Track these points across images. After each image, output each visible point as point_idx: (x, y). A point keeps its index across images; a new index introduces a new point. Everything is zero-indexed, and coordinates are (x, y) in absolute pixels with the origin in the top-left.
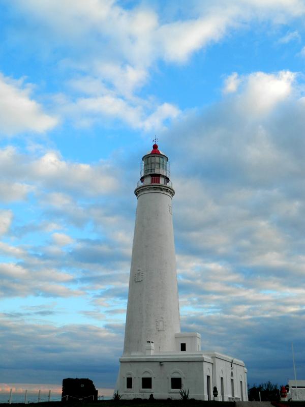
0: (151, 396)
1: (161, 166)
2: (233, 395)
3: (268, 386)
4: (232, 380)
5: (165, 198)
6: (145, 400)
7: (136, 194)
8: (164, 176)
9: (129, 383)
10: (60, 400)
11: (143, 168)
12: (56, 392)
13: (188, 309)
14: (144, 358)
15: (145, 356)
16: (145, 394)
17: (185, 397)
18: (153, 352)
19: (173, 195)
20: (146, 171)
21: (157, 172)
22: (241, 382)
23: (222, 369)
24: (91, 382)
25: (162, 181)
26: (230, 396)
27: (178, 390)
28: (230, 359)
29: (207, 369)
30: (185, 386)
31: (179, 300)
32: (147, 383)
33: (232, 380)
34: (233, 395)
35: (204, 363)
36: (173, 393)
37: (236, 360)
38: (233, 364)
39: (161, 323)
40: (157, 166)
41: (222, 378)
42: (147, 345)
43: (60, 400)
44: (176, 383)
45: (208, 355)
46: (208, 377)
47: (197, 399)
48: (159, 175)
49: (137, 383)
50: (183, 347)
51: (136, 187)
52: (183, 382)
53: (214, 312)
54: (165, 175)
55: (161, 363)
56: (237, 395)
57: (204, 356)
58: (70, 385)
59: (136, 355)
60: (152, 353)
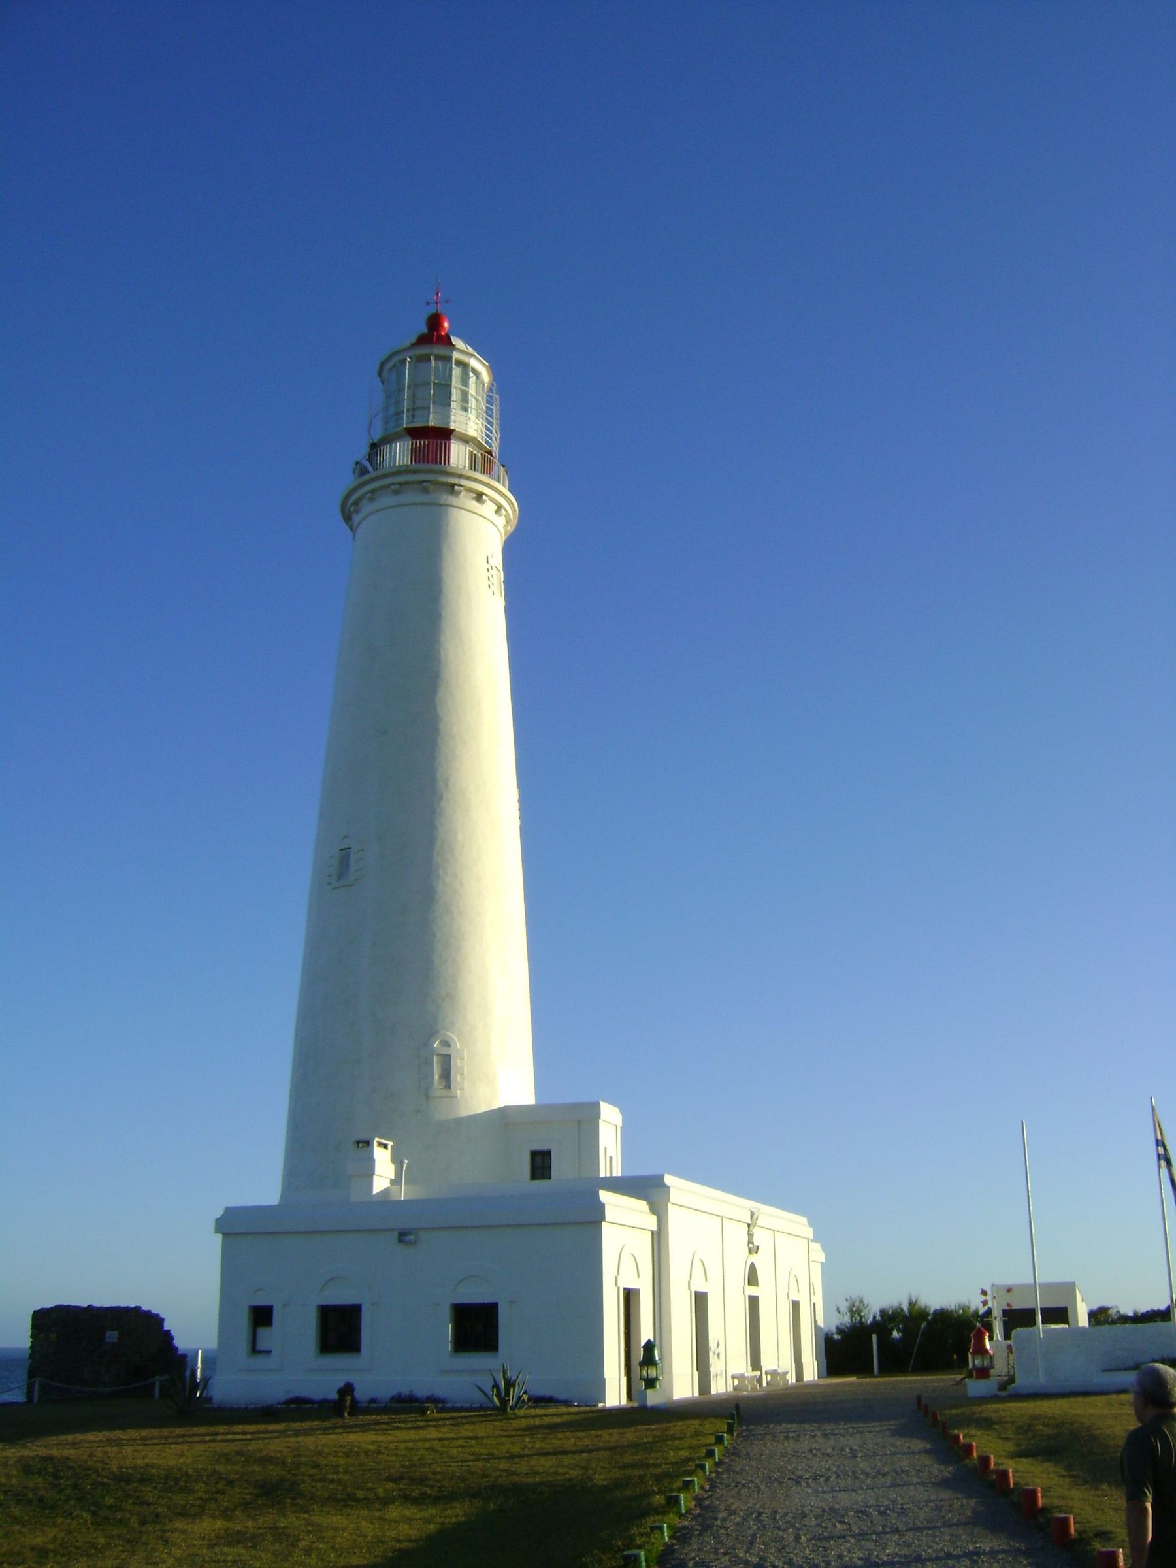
0: (347, 1389)
2: (756, 1362)
3: (851, 1311)
4: (753, 1302)
6: (323, 1402)
7: (347, 518)
16: (322, 1377)
22: (796, 1305)
33: (753, 1302)
34: (756, 1362)
36: (267, 1413)
38: (755, 1230)
44: (476, 1327)
46: (701, 1300)
49: (297, 1329)
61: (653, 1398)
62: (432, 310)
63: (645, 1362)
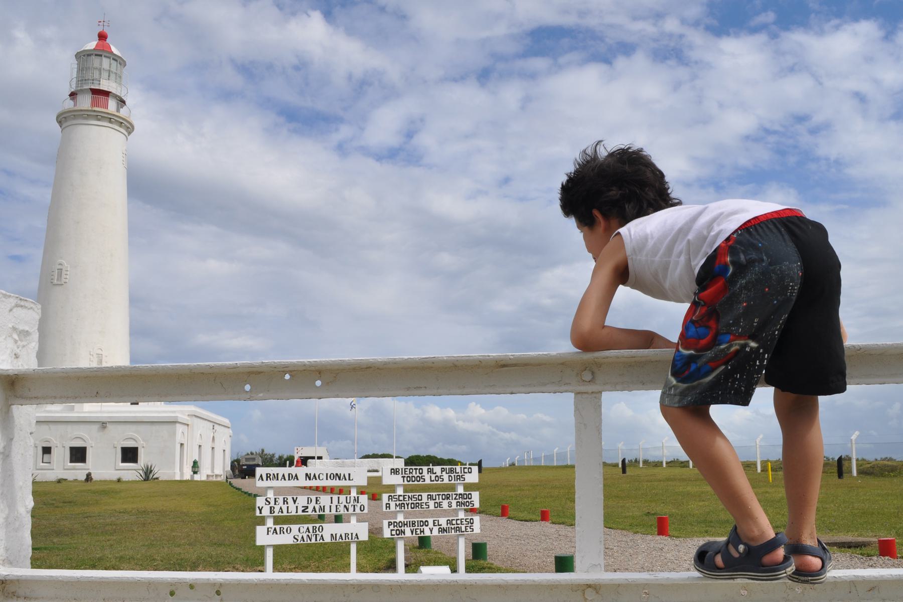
0: (89, 478)
8: (116, 97)
16: (78, 472)
19: (129, 133)
20: (81, 80)
25: (112, 105)
41: (200, 446)
46: (182, 445)
48: (106, 94)
49: (61, 455)
61: (197, 477)
62: (100, 29)
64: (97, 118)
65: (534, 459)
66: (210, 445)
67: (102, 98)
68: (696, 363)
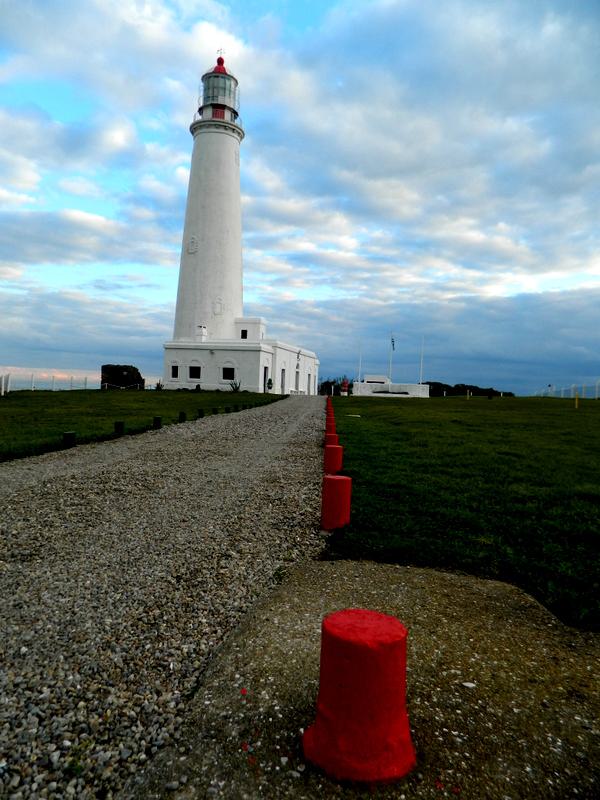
0: (198, 386)
1: (227, 92)
4: (297, 373)
5: (231, 140)
7: (192, 133)
8: (230, 109)
9: (175, 371)
10: (99, 388)
11: (202, 93)
12: (94, 379)
13: (249, 298)
14: (193, 344)
15: (372, 297)
16: (191, 384)
17: (236, 389)
18: (205, 338)
19: (242, 138)
20: (206, 98)
21: (220, 101)
23: (286, 361)
24: (135, 370)
25: (228, 115)
26: (294, 389)
27: (229, 381)
28: (298, 349)
29: (264, 360)
30: (237, 379)
31: (245, 275)
32: (195, 372)
33: (297, 373)
35: (261, 353)
37: (304, 351)
39: (218, 306)
40: (221, 92)
41: (283, 370)
42: (198, 331)
43: (99, 388)
44: (228, 373)
45: (269, 344)
46: (266, 368)
47: (251, 391)
48: (223, 107)
49: (184, 373)
50: (244, 334)
51: (192, 121)
52: (236, 372)
53: (27, 439)
54: (232, 106)
55: (212, 351)
56: (303, 388)
57: (261, 345)
58: (112, 374)
59: (184, 342)
60: (204, 339)
61: (270, 392)
63: (269, 384)
64: (218, 126)
65: (556, 392)
66: (294, 370)
67: (220, 110)
68: (477, 536)
